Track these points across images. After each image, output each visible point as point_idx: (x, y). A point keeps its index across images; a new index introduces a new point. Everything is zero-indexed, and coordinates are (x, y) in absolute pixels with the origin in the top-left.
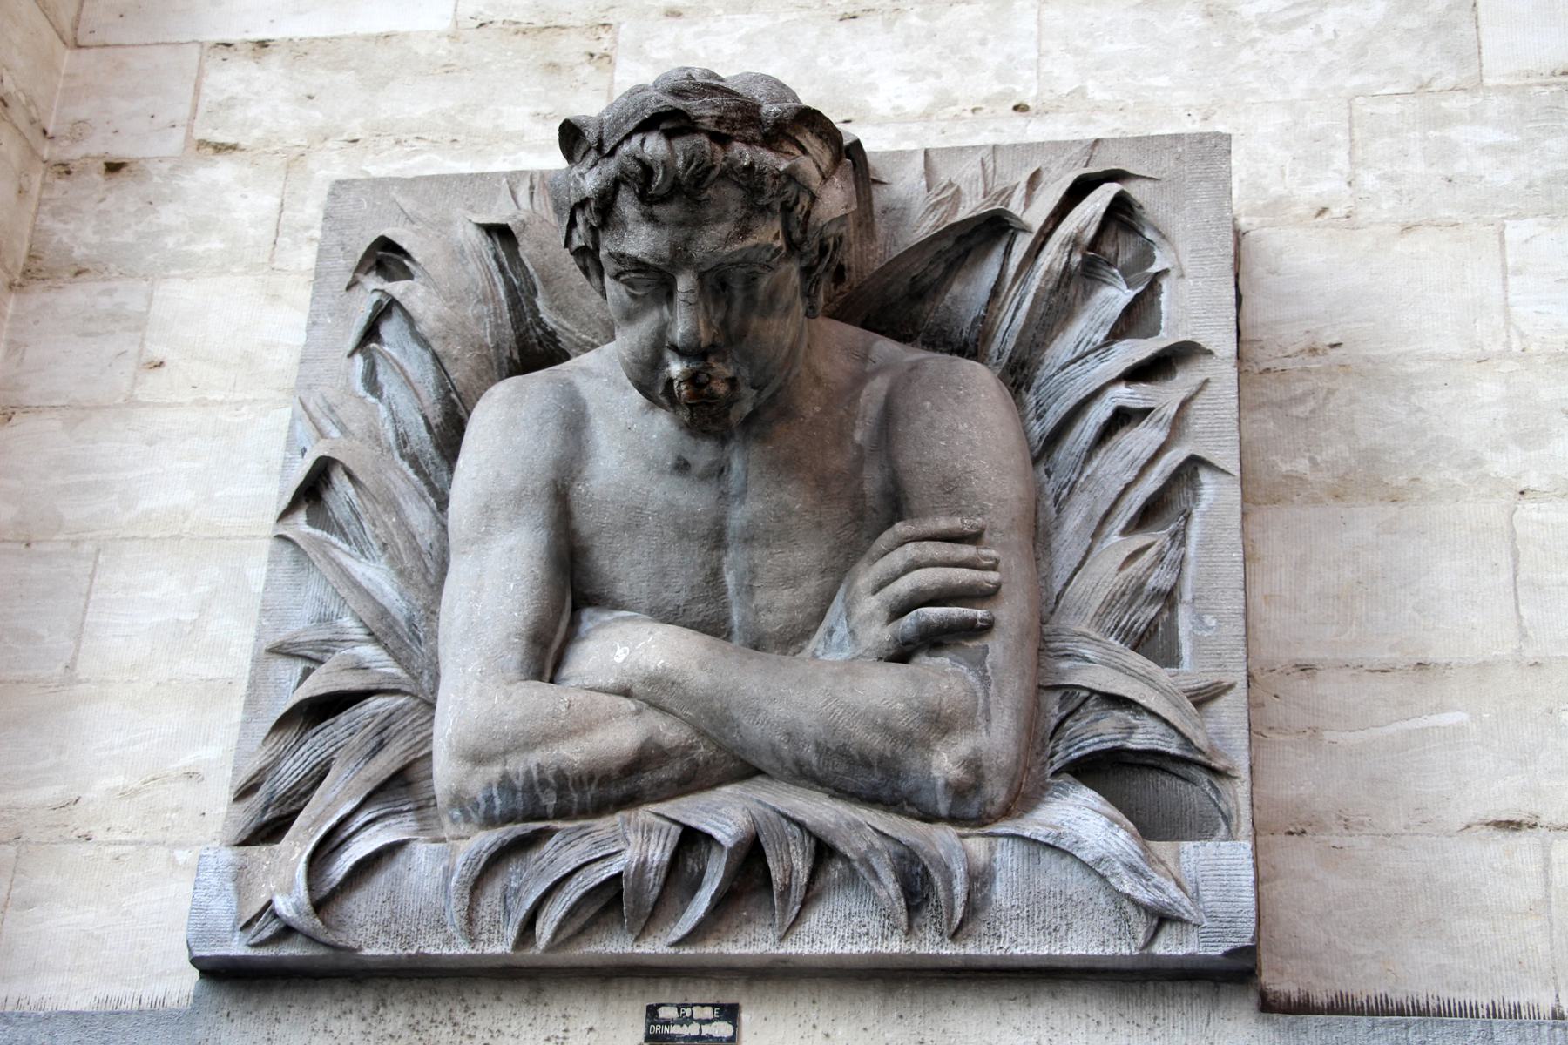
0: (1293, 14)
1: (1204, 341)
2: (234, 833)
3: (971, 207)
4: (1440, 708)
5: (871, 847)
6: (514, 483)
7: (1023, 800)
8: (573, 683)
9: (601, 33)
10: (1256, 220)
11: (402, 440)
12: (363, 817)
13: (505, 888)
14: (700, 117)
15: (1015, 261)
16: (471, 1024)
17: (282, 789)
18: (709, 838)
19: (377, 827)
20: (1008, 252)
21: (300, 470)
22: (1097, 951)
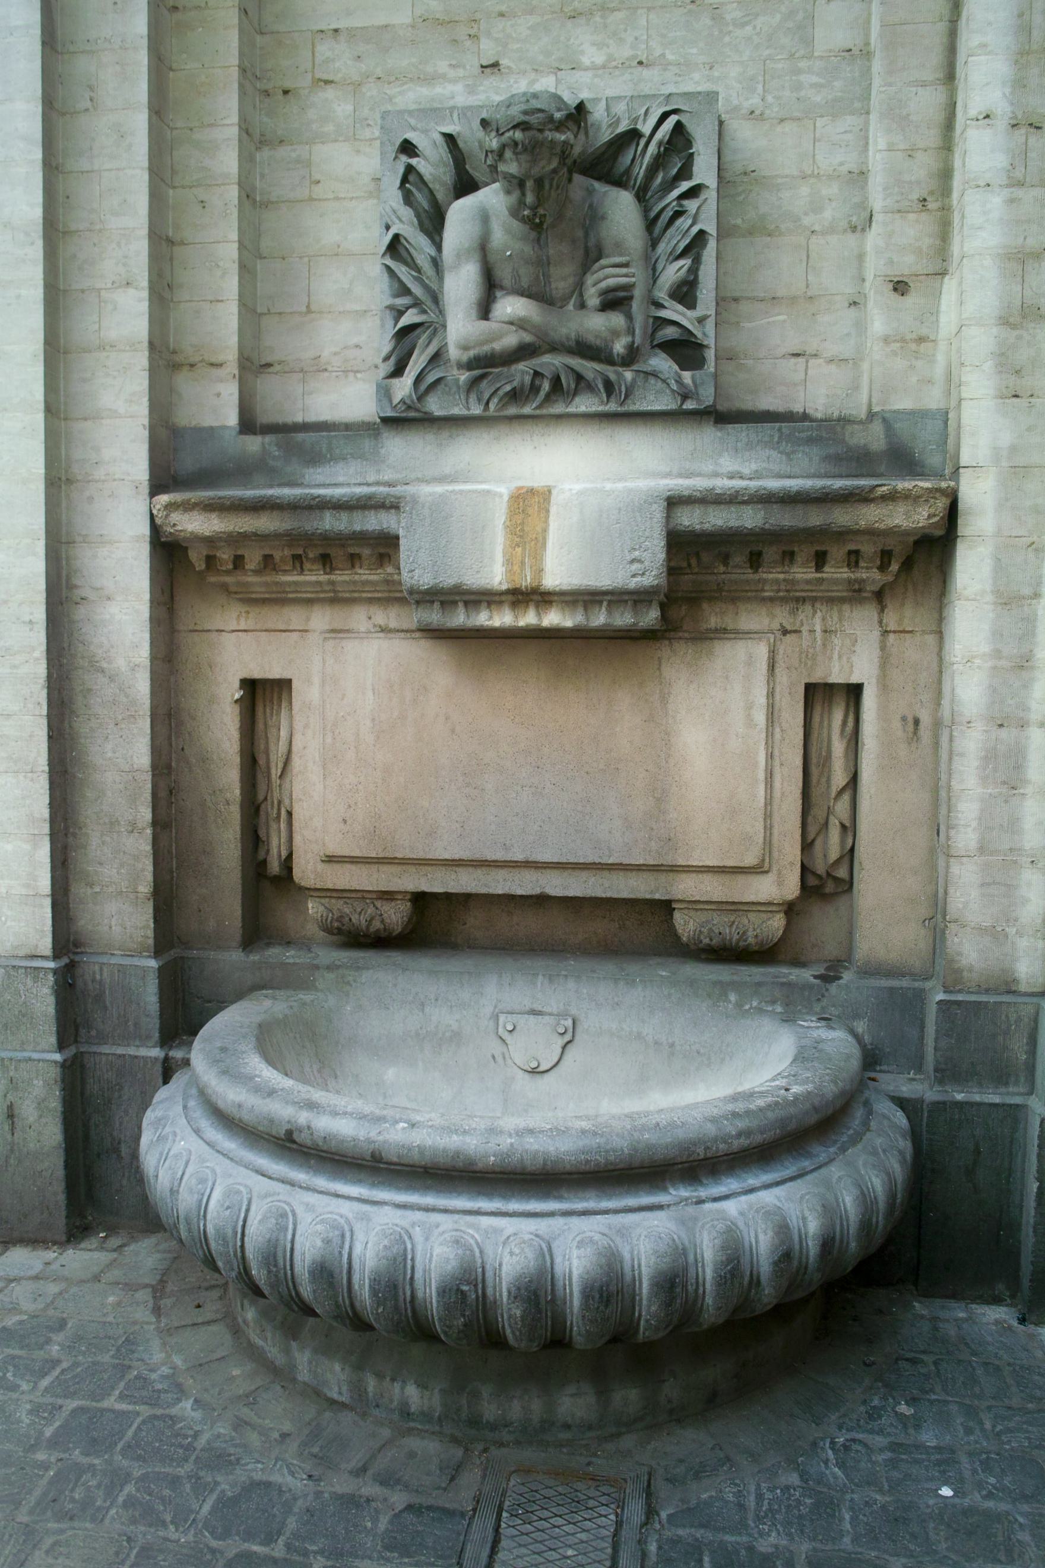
0: (746, 19)
3: (622, 128)
6: (466, 245)
10: (728, 116)
15: (640, 148)
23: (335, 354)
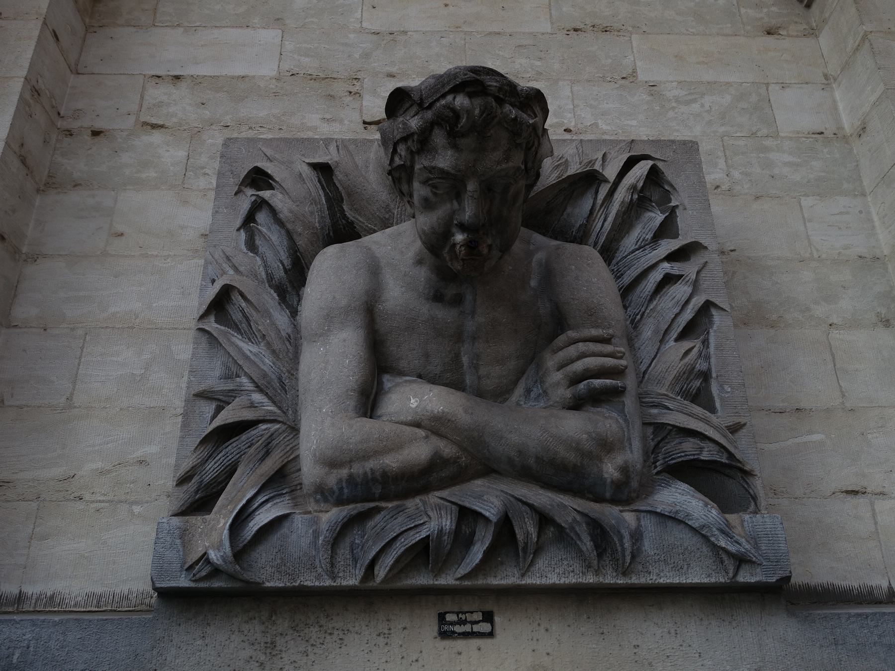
0: (690, 97)
1: (705, 241)
2: (176, 507)
4: (810, 432)
5: (575, 520)
6: (344, 303)
7: (647, 488)
8: (385, 418)
9: (355, 82)
11: (270, 277)
12: (261, 499)
13: (352, 544)
14: (490, 86)
16: (330, 626)
17: (207, 479)
18: (478, 515)
19: (269, 505)
20: (597, 192)
21: (212, 291)
22: (706, 581)
23: (102, 473)
